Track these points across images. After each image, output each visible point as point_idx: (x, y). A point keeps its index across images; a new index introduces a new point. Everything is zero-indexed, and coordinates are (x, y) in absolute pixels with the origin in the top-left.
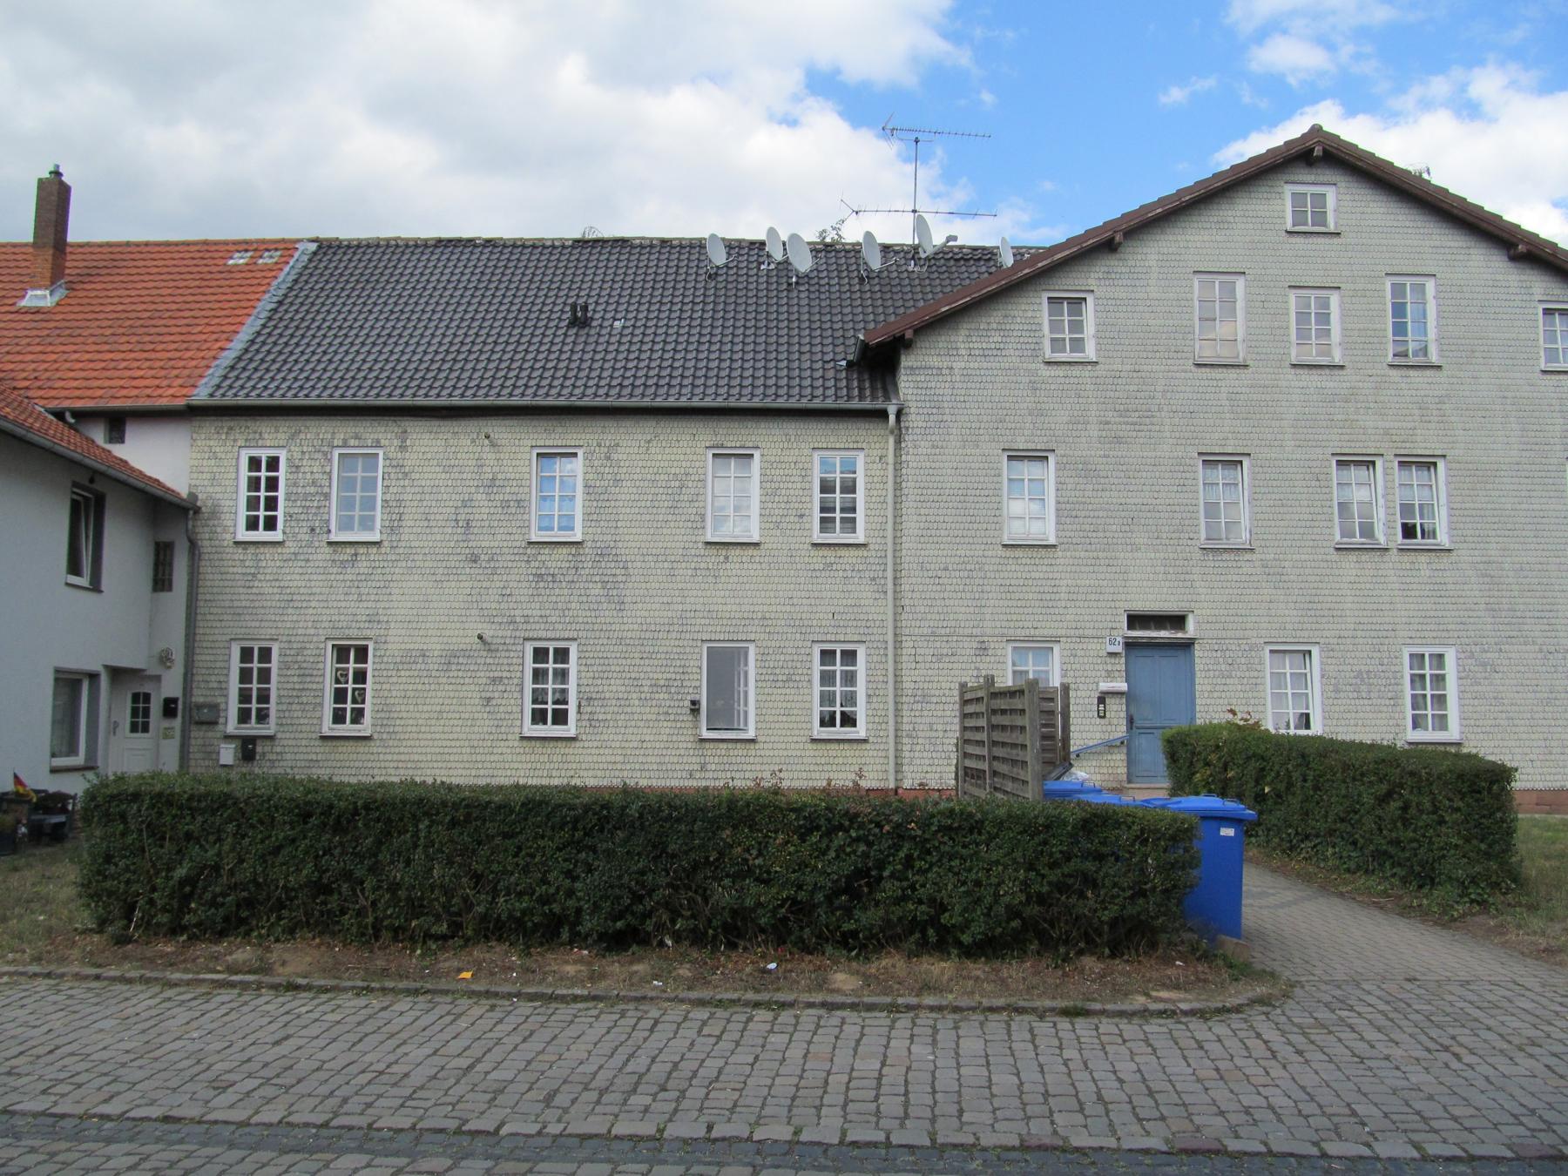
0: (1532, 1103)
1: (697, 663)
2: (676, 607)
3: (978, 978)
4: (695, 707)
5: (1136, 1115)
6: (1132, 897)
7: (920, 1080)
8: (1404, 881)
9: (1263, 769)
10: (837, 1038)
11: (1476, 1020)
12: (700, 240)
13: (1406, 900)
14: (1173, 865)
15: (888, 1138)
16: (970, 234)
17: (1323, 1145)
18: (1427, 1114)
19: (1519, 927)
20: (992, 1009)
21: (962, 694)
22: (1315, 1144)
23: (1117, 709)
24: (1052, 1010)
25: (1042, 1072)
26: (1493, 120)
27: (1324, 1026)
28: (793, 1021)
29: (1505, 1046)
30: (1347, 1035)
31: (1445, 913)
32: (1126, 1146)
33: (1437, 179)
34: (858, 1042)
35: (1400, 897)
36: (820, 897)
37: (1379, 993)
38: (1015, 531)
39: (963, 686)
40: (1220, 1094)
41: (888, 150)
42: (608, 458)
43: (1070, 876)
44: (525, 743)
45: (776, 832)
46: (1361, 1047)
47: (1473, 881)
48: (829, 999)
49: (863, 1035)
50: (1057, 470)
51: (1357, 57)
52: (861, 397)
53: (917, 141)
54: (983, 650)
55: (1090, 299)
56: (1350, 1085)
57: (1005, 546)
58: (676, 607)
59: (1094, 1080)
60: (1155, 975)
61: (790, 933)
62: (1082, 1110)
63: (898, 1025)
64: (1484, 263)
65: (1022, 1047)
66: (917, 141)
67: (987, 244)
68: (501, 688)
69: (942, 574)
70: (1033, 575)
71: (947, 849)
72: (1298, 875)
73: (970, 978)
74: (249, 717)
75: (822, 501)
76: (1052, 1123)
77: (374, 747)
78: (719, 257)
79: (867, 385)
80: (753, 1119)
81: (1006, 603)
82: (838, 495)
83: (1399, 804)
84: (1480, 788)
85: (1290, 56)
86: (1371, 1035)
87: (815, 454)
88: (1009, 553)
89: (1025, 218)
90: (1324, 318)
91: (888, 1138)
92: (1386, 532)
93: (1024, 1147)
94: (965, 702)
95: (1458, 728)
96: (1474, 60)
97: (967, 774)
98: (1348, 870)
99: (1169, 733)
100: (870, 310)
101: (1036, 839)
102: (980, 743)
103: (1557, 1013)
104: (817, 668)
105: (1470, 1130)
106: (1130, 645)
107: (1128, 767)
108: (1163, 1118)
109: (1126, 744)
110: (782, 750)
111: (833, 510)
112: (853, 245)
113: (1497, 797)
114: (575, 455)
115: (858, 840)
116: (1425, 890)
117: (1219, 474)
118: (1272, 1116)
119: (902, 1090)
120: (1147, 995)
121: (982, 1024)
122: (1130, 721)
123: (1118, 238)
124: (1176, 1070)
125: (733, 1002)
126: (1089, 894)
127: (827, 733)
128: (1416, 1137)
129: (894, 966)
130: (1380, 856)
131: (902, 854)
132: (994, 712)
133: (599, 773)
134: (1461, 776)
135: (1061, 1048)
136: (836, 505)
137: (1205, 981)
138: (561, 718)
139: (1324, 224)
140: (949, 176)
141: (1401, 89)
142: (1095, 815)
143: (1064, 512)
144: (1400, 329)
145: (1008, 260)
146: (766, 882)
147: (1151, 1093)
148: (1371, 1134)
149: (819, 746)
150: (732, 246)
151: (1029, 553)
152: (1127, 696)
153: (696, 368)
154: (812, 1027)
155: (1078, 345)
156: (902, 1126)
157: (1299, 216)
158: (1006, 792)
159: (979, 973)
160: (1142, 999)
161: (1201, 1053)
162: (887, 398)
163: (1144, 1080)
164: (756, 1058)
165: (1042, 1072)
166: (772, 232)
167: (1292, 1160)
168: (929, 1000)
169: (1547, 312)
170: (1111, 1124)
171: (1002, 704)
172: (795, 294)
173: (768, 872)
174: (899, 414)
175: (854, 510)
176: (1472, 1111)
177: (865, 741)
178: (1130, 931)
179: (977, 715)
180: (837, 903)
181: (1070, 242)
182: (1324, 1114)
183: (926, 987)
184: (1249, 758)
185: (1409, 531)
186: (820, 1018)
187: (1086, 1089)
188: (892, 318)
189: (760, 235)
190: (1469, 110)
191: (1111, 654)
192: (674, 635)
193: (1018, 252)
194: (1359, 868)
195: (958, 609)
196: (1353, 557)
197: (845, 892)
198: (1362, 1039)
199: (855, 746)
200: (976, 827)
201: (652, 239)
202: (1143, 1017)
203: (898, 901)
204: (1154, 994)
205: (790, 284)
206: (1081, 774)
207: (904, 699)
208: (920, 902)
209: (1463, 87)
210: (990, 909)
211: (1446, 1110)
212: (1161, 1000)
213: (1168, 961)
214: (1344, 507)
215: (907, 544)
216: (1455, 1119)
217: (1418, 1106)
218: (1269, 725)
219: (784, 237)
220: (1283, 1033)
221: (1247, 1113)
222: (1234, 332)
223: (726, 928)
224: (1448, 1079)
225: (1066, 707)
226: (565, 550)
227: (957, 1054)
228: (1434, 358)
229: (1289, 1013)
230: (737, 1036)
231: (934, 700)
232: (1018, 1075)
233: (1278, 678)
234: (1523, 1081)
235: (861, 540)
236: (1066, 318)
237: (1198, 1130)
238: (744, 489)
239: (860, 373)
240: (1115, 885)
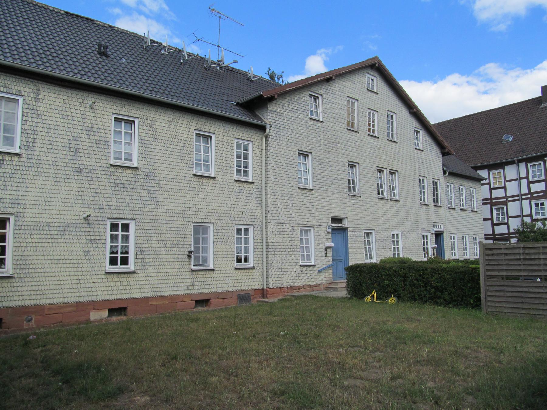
42: (151, 127)
44: (108, 276)
66: (220, 18)
68: (94, 245)
77: (15, 283)
104: (109, 233)
106: (334, 229)
123: (334, 77)
127: (239, 265)
133: (146, 290)
138: (125, 261)
215: (270, 184)
226: (129, 171)
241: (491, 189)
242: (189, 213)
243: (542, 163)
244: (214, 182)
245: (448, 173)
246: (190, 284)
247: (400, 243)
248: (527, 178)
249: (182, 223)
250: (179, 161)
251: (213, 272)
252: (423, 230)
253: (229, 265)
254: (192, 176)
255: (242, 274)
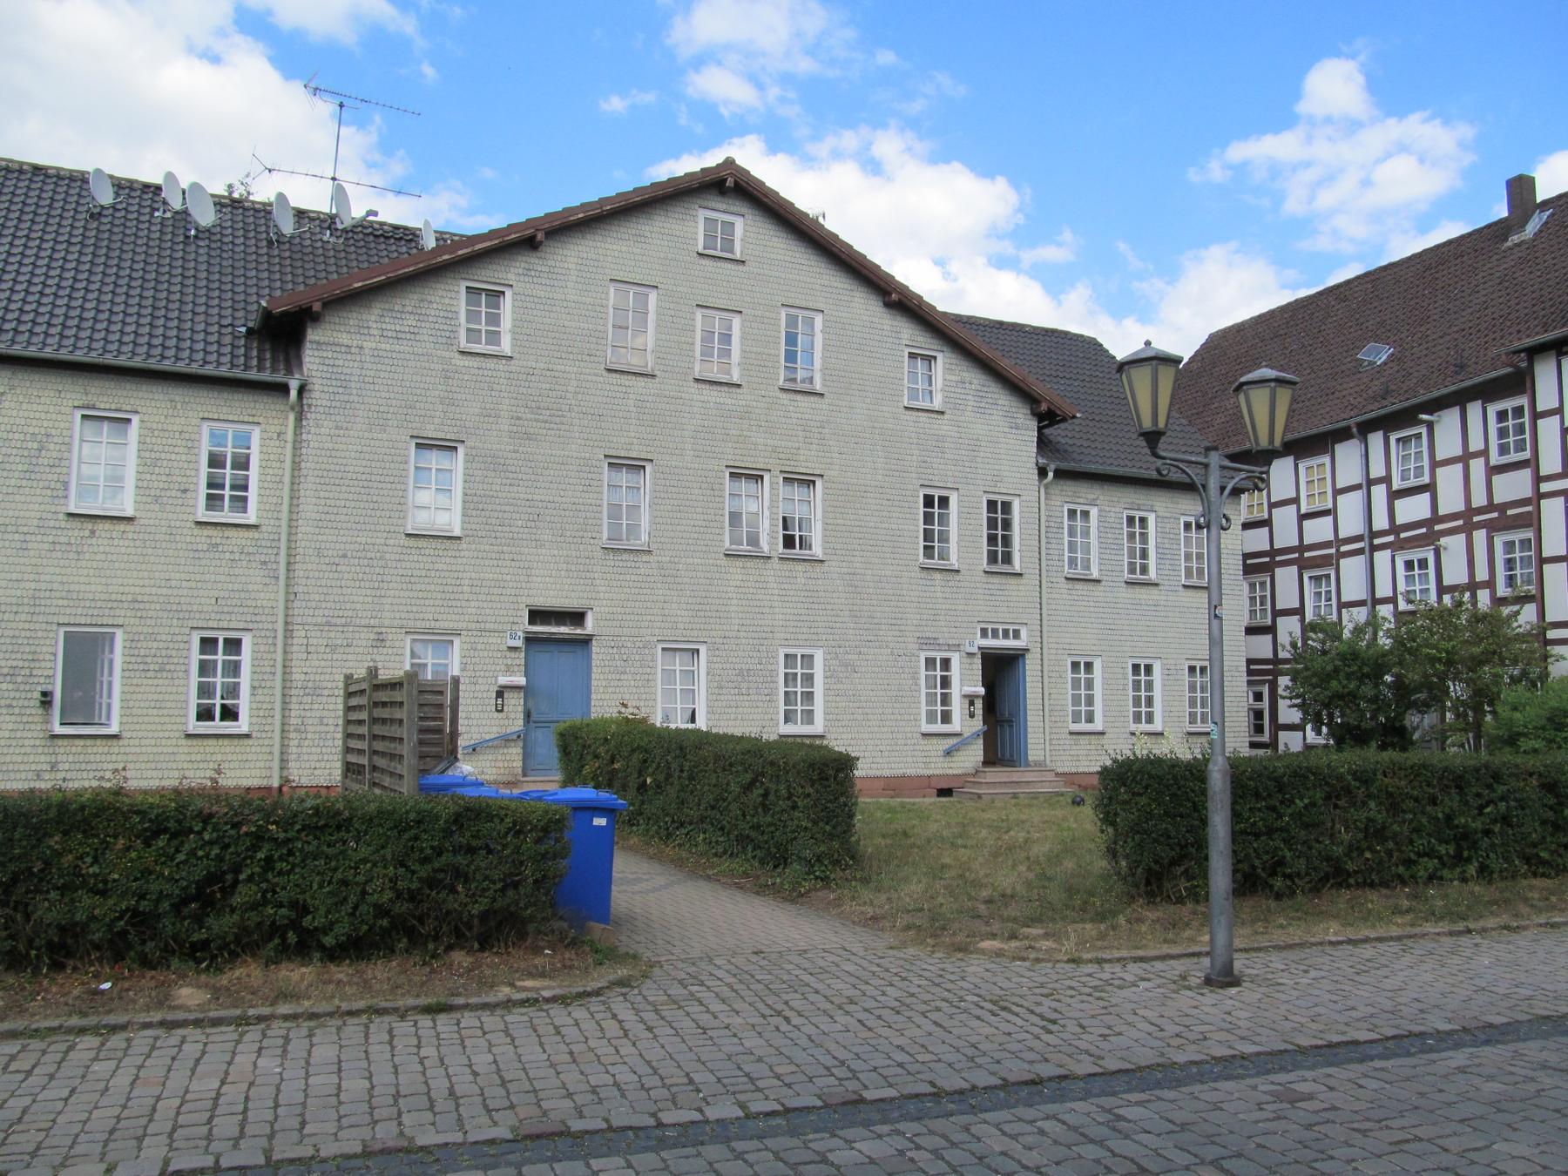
0: (842, 1054)
1: (51, 650)
2: (27, 585)
3: (339, 981)
4: (46, 699)
5: (486, 1107)
6: (503, 890)
7: (263, 1094)
8: (762, 862)
9: (645, 761)
10: (173, 1059)
11: (807, 985)
12: (83, 173)
13: (762, 880)
14: (544, 856)
15: (217, 1162)
16: (393, 212)
17: (660, 1115)
18: (755, 1076)
19: (853, 898)
20: (350, 1013)
21: (347, 685)
22: (654, 1115)
23: (515, 703)
24: (415, 1008)
25: (396, 1072)
26: (890, 180)
27: (675, 1002)
28: (124, 1045)
29: (828, 1006)
30: (694, 1009)
31: (794, 890)
32: (471, 1138)
33: (830, 225)
34: (198, 1061)
35: (758, 877)
36: (165, 905)
37: (728, 967)
38: (419, 520)
39: (348, 678)
40: (571, 1077)
41: (325, 108)
43: (441, 870)
45: (116, 837)
46: (705, 1019)
47: (819, 859)
48: (170, 1017)
49: (204, 1053)
50: (466, 461)
51: (782, 100)
52: (260, 368)
53: (341, 106)
54: (380, 641)
55: (509, 293)
56: (692, 1056)
57: (409, 535)
58: (27, 585)
59: (448, 1076)
60: (523, 965)
61: (130, 947)
62: (431, 1108)
63: (245, 1038)
64: (864, 307)
65: (379, 1052)
67: (411, 224)
69: (342, 561)
70: (437, 566)
71: (311, 848)
72: (672, 861)
73: (330, 982)
74: (1193, 851)
75: (210, 475)
76: (400, 1124)
78: (105, 197)
79: (268, 355)
80: (59, 1160)
81: (407, 594)
82: (228, 471)
83: (761, 791)
84: (827, 773)
85: (722, 86)
86: (716, 1007)
87: (202, 425)
88: (412, 542)
89: (463, 202)
90: (726, 338)
91: (217, 1162)
92: (770, 542)
93: (367, 1154)
94: (349, 695)
95: (820, 723)
96: (879, 124)
97: (350, 769)
98: (716, 855)
99: (562, 726)
100: (277, 276)
101: (406, 836)
102: (361, 737)
103: (874, 973)
104: (196, 656)
105: (789, 1086)
106: (531, 640)
107: (524, 760)
108: (512, 1107)
109: (523, 738)
110: (149, 747)
111: (222, 487)
112: (264, 204)
113: (841, 784)
114: (129, 420)
115: (211, 843)
116: (779, 870)
117: (624, 477)
118: (617, 1093)
119: (241, 1108)
120: (512, 985)
121: (339, 1029)
122: (528, 715)
123: (540, 236)
124: (532, 1058)
125: (52, 1030)
126: (460, 888)
128: (742, 1097)
129: (249, 976)
130: (743, 839)
131: (260, 855)
132: (376, 704)
134: (812, 765)
135: (419, 1047)
136: (226, 480)
137: (571, 967)
139: (732, 252)
140: (387, 147)
141: (816, 138)
142: (468, 809)
143: (471, 505)
144: (791, 357)
145: (430, 243)
146: (103, 893)
147: (503, 1083)
148: (704, 1099)
149: (194, 742)
150: (120, 185)
151: (433, 543)
152: (526, 690)
153: (66, 316)
154: (146, 1050)
155: (494, 337)
156: (235, 1146)
157: (710, 238)
158: (384, 787)
159: (341, 976)
160: (507, 990)
161: (558, 1038)
162: (289, 372)
163: (499, 1070)
164: (73, 1091)
165: (396, 1072)
166: (170, 177)
167: (630, 1133)
168: (284, 1009)
169: (912, 356)
170: (460, 1119)
171: (383, 696)
172: (193, 248)
173: (105, 882)
174: (302, 390)
175: (246, 488)
176: (794, 1068)
177: (247, 736)
178: (500, 923)
179: (360, 708)
180: (185, 911)
181: (493, 234)
182: (664, 1086)
183: (284, 996)
184: (633, 751)
185: (789, 542)
186: (156, 1038)
187: (439, 1086)
188: (302, 287)
189: (155, 178)
190: (873, 167)
191: (511, 649)
192: (23, 617)
193: (441, 236)
194: (725, 852)
195: (356, 599)
196: (740, 563)
197: (195, 898)
198: (708, 1011)
199: (236, 742)
200: (343, 825)
201: (22, 164)
202: (507, 1007)
203: (254, 907)
204: (519, 984)
205: (187, 237)
206: (466, 768)
207: (293, 692)
208: (281, 906)
209: (868, 145)
210: (356, 908)
211: (739, 1068)
212: (525, 989)
213: (537, 951)
214: (735, 517)
215: (304, 528)
216: (778, 1077)
217: (747, 1068)
218: (658, 721)
219: (184, 185)
220: (637, 1012)
221: (594, 1092)
222: (646, 345)
223: (51, 947)
224: (778, 1041)
225: (455, 700)
227: (308, 1063)
228: (818, 387)
229: (645, 992)
230: (52, 1069)
231: (326, 692)
232: (370, 1078)
233: (669, 675)
234: (839, 1037)
235: (252, 520)
236: (484, 309)
237: (545, 1114)
238: (118, 455)
239: (261, 342)
240: (486, 878)
241: (1302, 517)
242: (48, 602)
243: (1423, 430)
244: (129, 528)
245: (1051, 475)
246: (45, 767)
247: (1157, 685)
248: (1387, 480)
249: (27, 626)
250: (24, 483)
251: (115, 742)
252: (927, 642)
253: (170, 727)
254: (61, 516)
255: (208, 750)
